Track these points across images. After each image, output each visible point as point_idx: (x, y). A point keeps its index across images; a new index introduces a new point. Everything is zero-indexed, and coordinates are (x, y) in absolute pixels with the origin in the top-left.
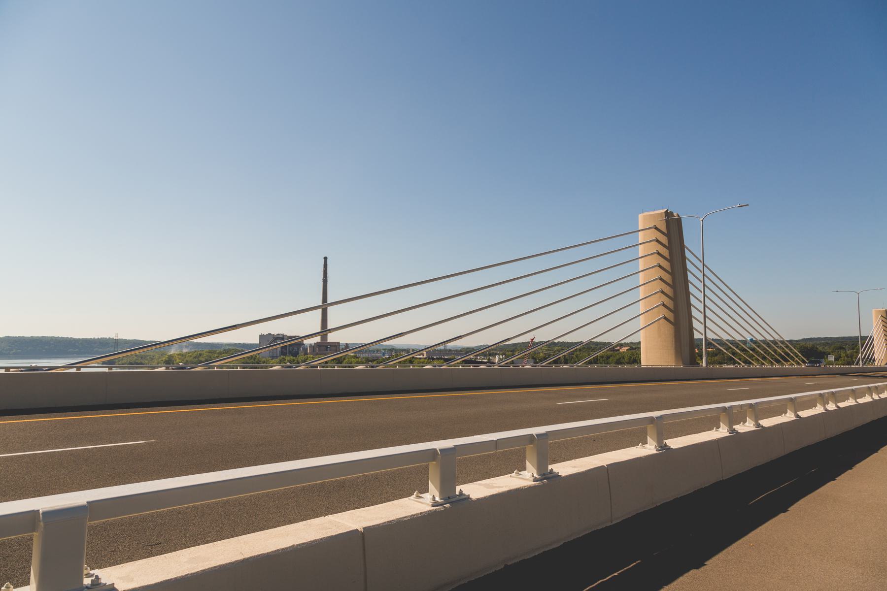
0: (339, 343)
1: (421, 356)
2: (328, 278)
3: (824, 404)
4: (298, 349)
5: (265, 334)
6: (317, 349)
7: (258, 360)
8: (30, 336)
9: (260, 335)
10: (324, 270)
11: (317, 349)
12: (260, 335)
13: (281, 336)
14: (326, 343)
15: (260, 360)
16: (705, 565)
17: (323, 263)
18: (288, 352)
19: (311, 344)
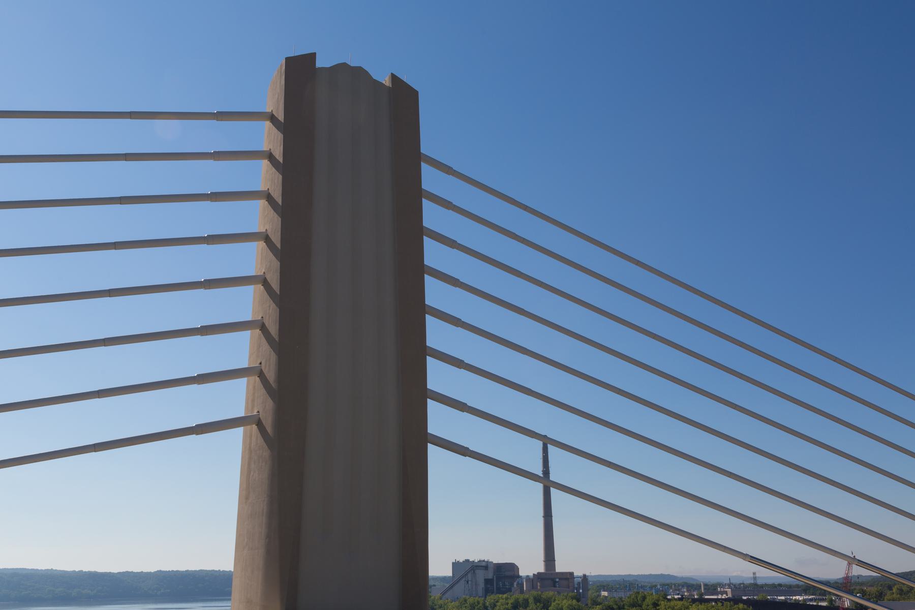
0: (572, 574)
1: (724, 596)
2: (550, 469)
3: (722, 595)
4: (512, 585)
5: (461, 561)
6: (539, 584)
7: (433, 603)
8: (139, 571)
9: (453, 563)
10: (544, 456)
11: (539, 584)
12: (453, 563)
13: (484, 564)
14: (552, 574)
15: (436, 602)
16: (394, 78)
17: (113, 251)
18: (495, 589)
19: (528, 576)
